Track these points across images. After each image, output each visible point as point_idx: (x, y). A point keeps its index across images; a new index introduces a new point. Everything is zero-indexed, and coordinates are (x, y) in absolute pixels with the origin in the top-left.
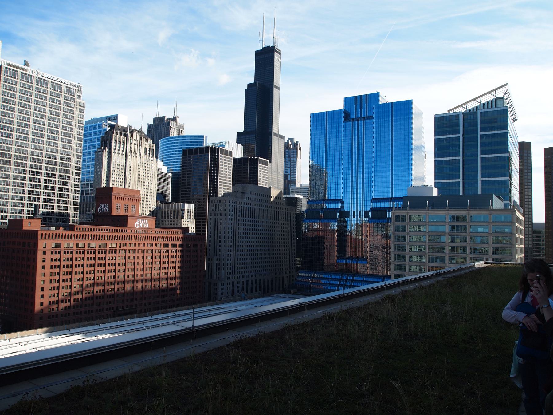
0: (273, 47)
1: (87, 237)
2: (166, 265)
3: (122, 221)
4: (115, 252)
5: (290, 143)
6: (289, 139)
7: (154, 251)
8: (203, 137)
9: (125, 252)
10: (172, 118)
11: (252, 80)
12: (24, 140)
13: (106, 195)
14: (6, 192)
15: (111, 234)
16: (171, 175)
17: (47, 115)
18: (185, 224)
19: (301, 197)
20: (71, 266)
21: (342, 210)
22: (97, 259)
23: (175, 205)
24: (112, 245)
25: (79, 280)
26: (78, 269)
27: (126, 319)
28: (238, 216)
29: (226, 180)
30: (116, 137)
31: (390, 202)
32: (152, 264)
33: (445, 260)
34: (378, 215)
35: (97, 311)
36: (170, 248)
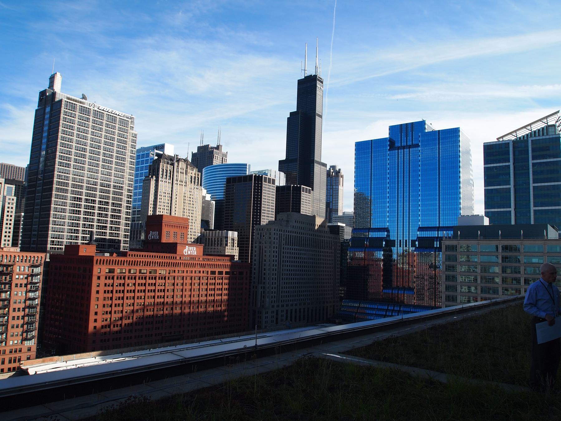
0: (315, 76)
2: (213, 292)
3: (172, 248)
4: (165, 278)
5: (332, 171)
6: (331, 167)
8: (246, 165)
9: (174, 279)
10: (216, 146)
13: (156, 222)
14: (63, 219)
15: (161, 261)
16: (214, 202)
17: (102, 145)
18: (229, 251)
19: (344, 225)
21: (388, 239)
22: (147, 285)
23: (219, 232)
24: (162, 271)
25: (130, 305)
26: (129, 295)
27: (176, 345)
29: (269, 208)
30: (163, 166)
31: (438, 231)
33: (498, 290)
34: (425, 245)
35: (135, 337)
36: (217, 275)
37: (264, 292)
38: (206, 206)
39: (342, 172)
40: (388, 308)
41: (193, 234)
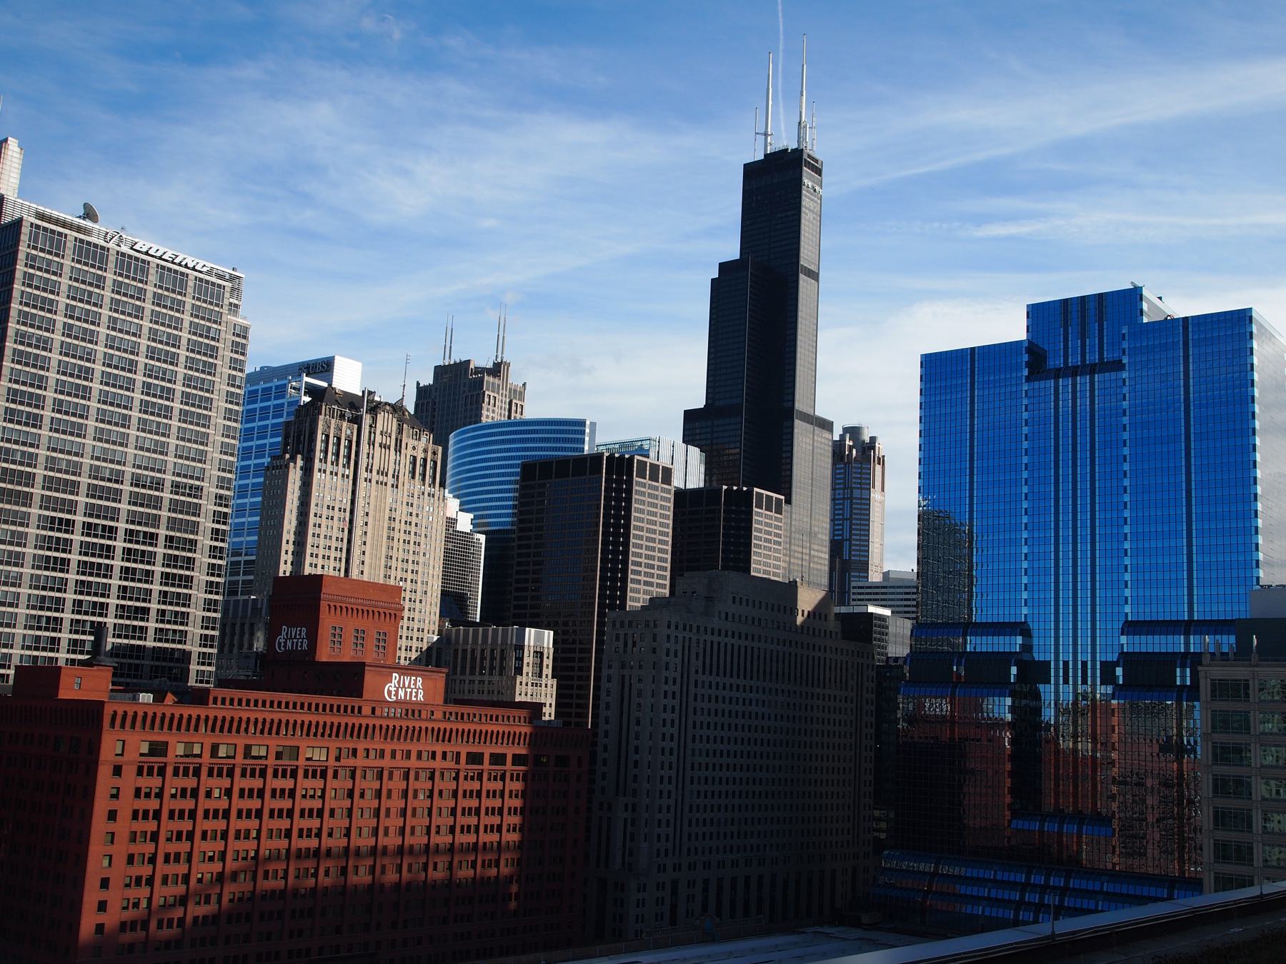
0: (798, 152)
1: (244, 726)
2: (473, 820)
3: (348, 679)
4: (324, 775)
5: (848, 443)
6: (846, 430)
7: (437, 774)
9: (353, 777)
10: (490, 365)
11: (732, 251)
12: (72, 434)
13: (302, 597)
14: (13, 585)
15: (314, 718)
16: (482, 538)
17: (142, 360)
18: (524, 691)
19: (887, 612)
20: (193, 814)
21: (1026, 657)
22: (268, 795)
24: (315, 752)
25: (211, 859)
26: (210, 825)
28: (693, 670)
29: (652, 558)
30: (327, 425)
31: (1187, 634)
32: (430, 815)
34: (1145, 677)
36: (486, 765)
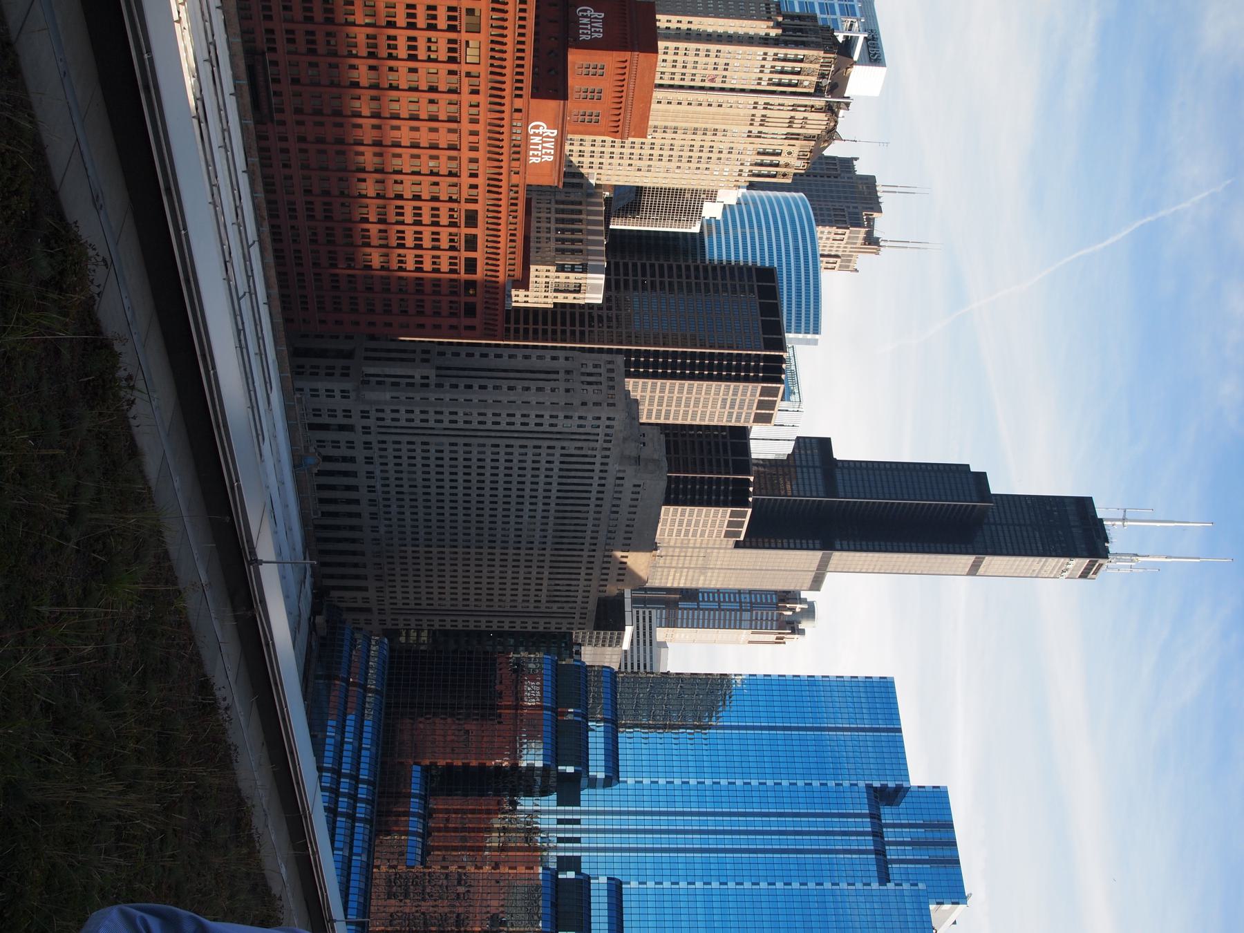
3: (550, 82)
4: (452, 60)
5: (798, 607)
6: (811, 605)
8: (816, 331)
9: (451, 91)
10: (876, 234)
15: (509, 47)
16: (696, 229)
18: (541, 274)
19: (626, 645)
21: (584, 782)
24: (475, 51)
27: (237, 92)
30: (814, 59)
36: (465, 231)
37: (412, 385)
38: (683, 201)
39: (793, 641)
40: (363, 782)
41: (596, 160)
